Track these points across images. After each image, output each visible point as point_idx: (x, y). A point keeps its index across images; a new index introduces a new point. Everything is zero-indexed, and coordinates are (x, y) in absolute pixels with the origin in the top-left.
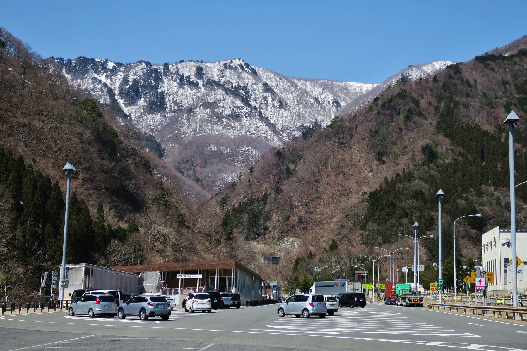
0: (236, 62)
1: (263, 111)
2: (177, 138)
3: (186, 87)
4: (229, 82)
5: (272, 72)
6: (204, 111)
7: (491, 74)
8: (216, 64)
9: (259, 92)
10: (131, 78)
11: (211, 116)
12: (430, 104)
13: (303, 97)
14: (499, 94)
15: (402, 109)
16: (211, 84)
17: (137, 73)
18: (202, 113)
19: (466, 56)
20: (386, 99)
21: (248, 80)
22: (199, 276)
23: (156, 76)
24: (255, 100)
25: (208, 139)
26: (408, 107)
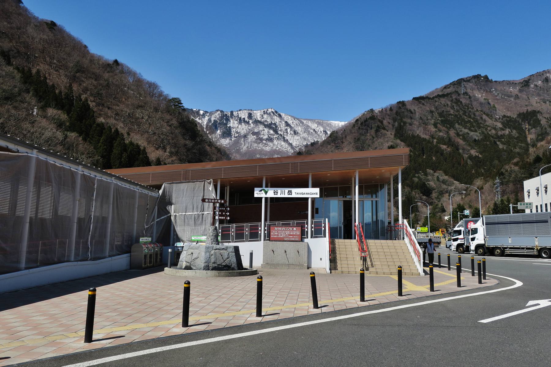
0: (270, 110)
1: (285, 136)
2: (238, 151)
3: (243, 124)
4: (266, 121)
5: (290, 116)
6: (253, 137)
7: (423, 107)
8: (259, 111)
9: (283, 126)
10: (213, 119)
11: (256, 139)
12: (389, 123)
13: (307, 129)
14: (429, 117)
15: (373, 126)
16: (257, 122)
17: (216, 116)
18: (252, 138)
19: (407, 97)
20: (363, 120)
21: (277, 120)
22: (311, 193)
23: (226, 118)
24: (281, 130)
25: (255, 151)
26: (376, 125)
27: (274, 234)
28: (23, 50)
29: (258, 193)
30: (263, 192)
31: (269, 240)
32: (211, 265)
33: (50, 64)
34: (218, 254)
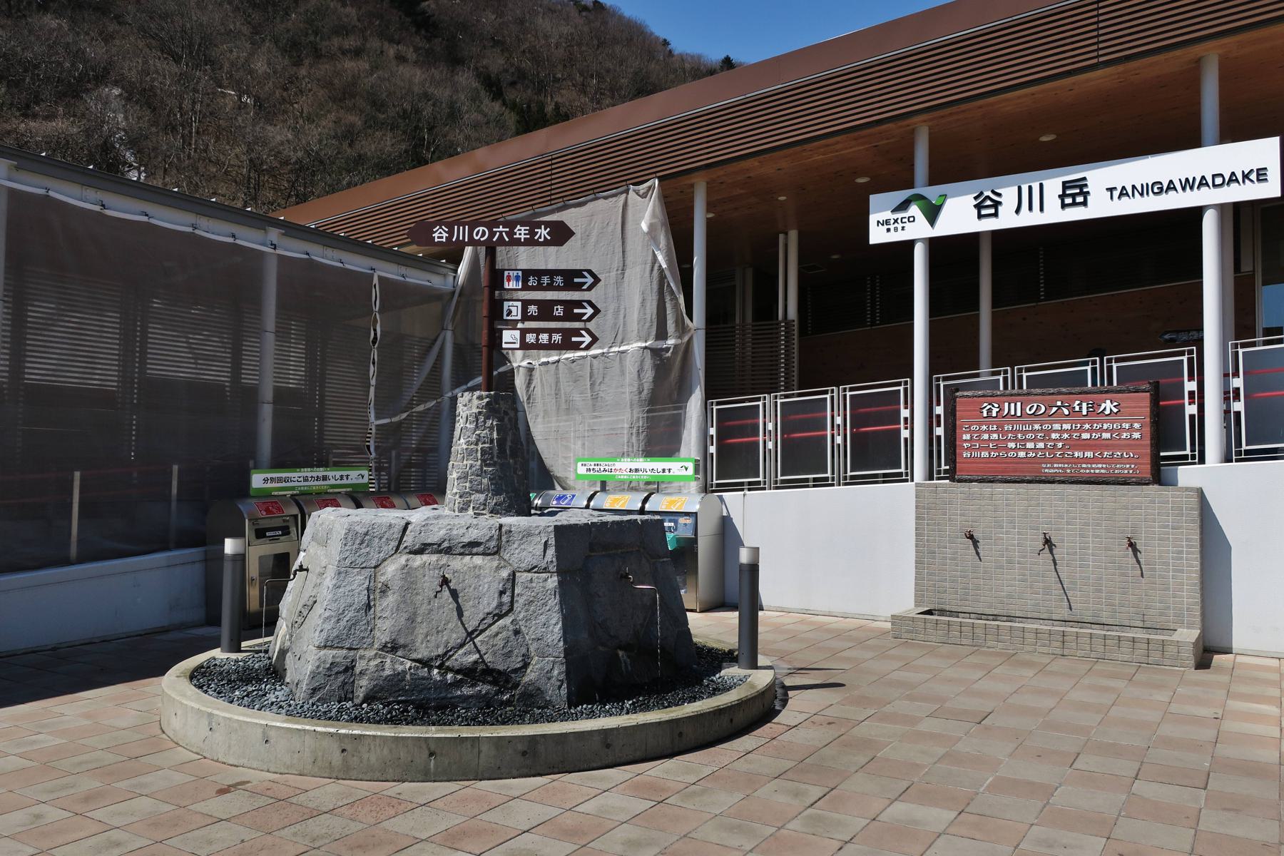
27: (978, 439)
28: (527, 64)
29: (886, 224)
30: (914, 210)
31: (951, 475)
32: (372, 666)
33: (583, 89)
34: (429, 583)
